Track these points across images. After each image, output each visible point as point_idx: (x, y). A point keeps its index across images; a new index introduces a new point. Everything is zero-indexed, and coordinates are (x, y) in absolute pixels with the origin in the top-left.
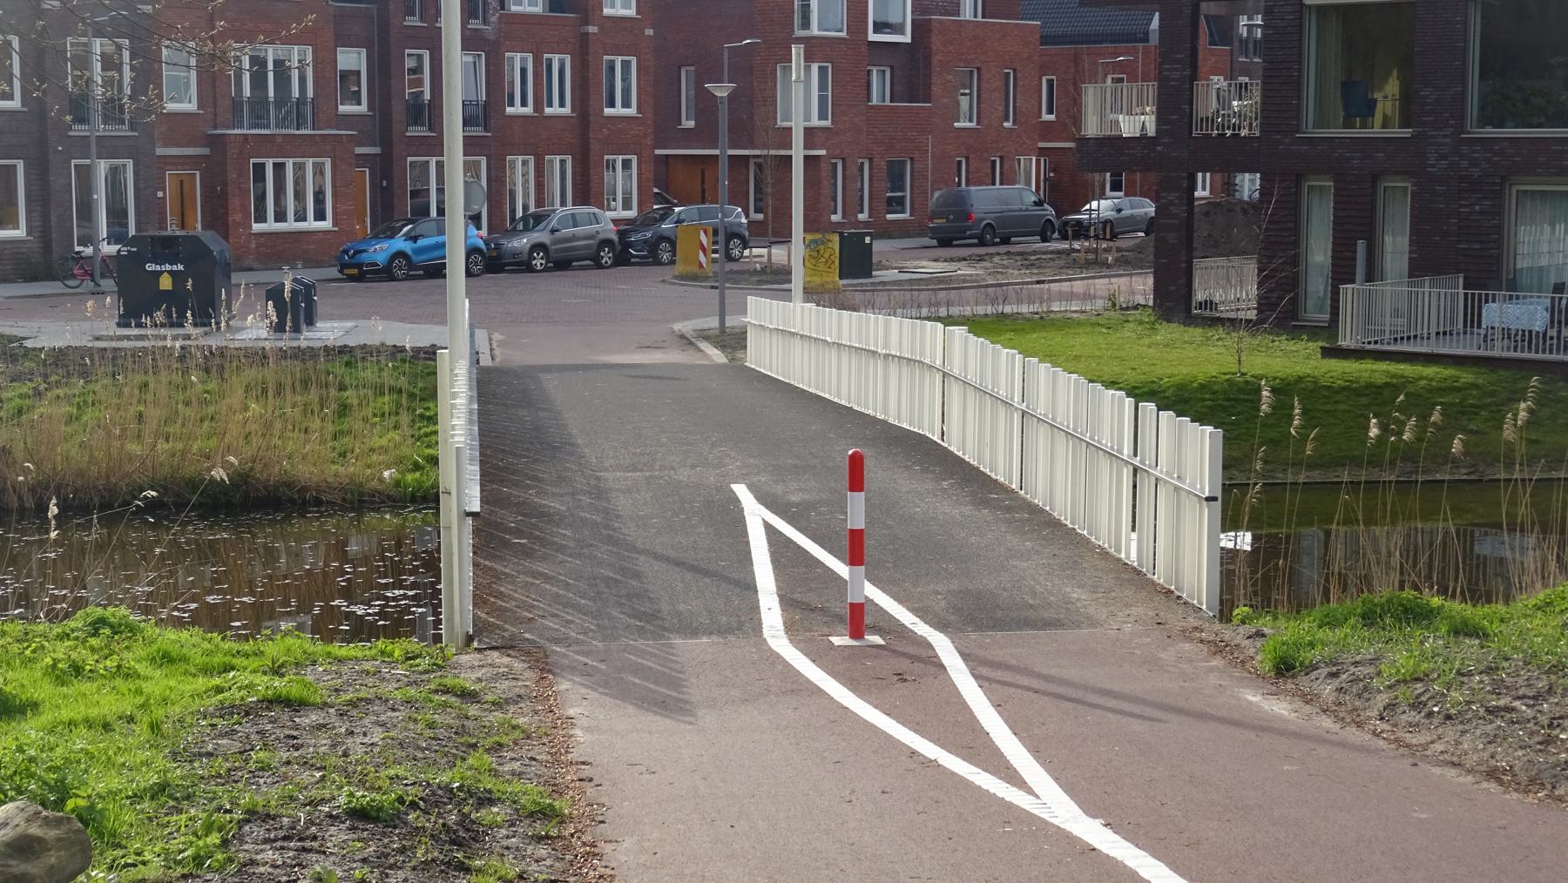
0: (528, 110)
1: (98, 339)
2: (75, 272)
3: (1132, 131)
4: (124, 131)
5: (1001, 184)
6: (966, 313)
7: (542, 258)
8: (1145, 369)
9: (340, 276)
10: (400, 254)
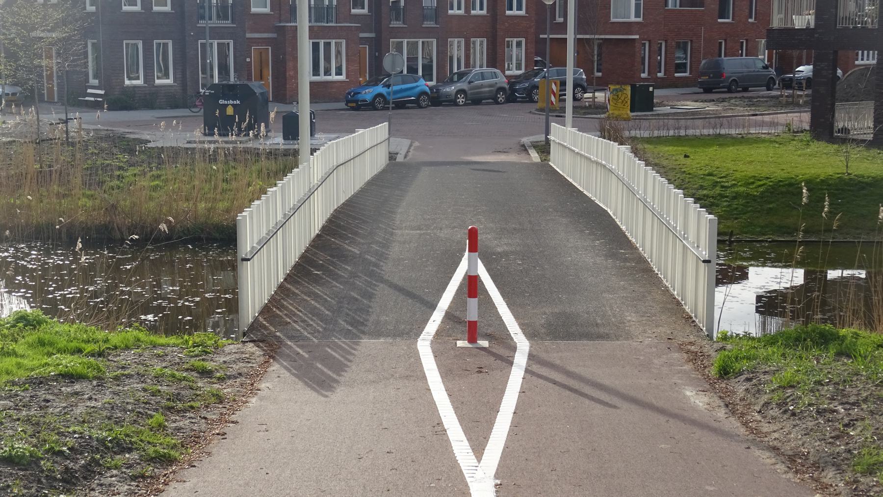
0: (461, 12)
1: (189, 142)
2: (197, 104)
3: (800, 25)
4: (228, 23)
5: (746, 56)
6: (697, 134)
7: (463, 98)
8: (790, 170)
9: (346, 107)
10: (380, 95)
